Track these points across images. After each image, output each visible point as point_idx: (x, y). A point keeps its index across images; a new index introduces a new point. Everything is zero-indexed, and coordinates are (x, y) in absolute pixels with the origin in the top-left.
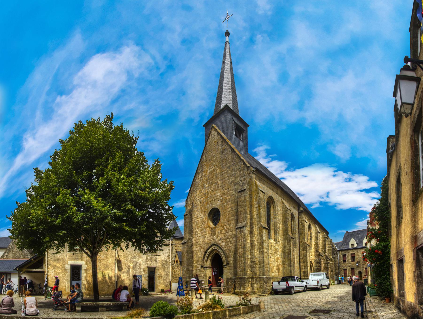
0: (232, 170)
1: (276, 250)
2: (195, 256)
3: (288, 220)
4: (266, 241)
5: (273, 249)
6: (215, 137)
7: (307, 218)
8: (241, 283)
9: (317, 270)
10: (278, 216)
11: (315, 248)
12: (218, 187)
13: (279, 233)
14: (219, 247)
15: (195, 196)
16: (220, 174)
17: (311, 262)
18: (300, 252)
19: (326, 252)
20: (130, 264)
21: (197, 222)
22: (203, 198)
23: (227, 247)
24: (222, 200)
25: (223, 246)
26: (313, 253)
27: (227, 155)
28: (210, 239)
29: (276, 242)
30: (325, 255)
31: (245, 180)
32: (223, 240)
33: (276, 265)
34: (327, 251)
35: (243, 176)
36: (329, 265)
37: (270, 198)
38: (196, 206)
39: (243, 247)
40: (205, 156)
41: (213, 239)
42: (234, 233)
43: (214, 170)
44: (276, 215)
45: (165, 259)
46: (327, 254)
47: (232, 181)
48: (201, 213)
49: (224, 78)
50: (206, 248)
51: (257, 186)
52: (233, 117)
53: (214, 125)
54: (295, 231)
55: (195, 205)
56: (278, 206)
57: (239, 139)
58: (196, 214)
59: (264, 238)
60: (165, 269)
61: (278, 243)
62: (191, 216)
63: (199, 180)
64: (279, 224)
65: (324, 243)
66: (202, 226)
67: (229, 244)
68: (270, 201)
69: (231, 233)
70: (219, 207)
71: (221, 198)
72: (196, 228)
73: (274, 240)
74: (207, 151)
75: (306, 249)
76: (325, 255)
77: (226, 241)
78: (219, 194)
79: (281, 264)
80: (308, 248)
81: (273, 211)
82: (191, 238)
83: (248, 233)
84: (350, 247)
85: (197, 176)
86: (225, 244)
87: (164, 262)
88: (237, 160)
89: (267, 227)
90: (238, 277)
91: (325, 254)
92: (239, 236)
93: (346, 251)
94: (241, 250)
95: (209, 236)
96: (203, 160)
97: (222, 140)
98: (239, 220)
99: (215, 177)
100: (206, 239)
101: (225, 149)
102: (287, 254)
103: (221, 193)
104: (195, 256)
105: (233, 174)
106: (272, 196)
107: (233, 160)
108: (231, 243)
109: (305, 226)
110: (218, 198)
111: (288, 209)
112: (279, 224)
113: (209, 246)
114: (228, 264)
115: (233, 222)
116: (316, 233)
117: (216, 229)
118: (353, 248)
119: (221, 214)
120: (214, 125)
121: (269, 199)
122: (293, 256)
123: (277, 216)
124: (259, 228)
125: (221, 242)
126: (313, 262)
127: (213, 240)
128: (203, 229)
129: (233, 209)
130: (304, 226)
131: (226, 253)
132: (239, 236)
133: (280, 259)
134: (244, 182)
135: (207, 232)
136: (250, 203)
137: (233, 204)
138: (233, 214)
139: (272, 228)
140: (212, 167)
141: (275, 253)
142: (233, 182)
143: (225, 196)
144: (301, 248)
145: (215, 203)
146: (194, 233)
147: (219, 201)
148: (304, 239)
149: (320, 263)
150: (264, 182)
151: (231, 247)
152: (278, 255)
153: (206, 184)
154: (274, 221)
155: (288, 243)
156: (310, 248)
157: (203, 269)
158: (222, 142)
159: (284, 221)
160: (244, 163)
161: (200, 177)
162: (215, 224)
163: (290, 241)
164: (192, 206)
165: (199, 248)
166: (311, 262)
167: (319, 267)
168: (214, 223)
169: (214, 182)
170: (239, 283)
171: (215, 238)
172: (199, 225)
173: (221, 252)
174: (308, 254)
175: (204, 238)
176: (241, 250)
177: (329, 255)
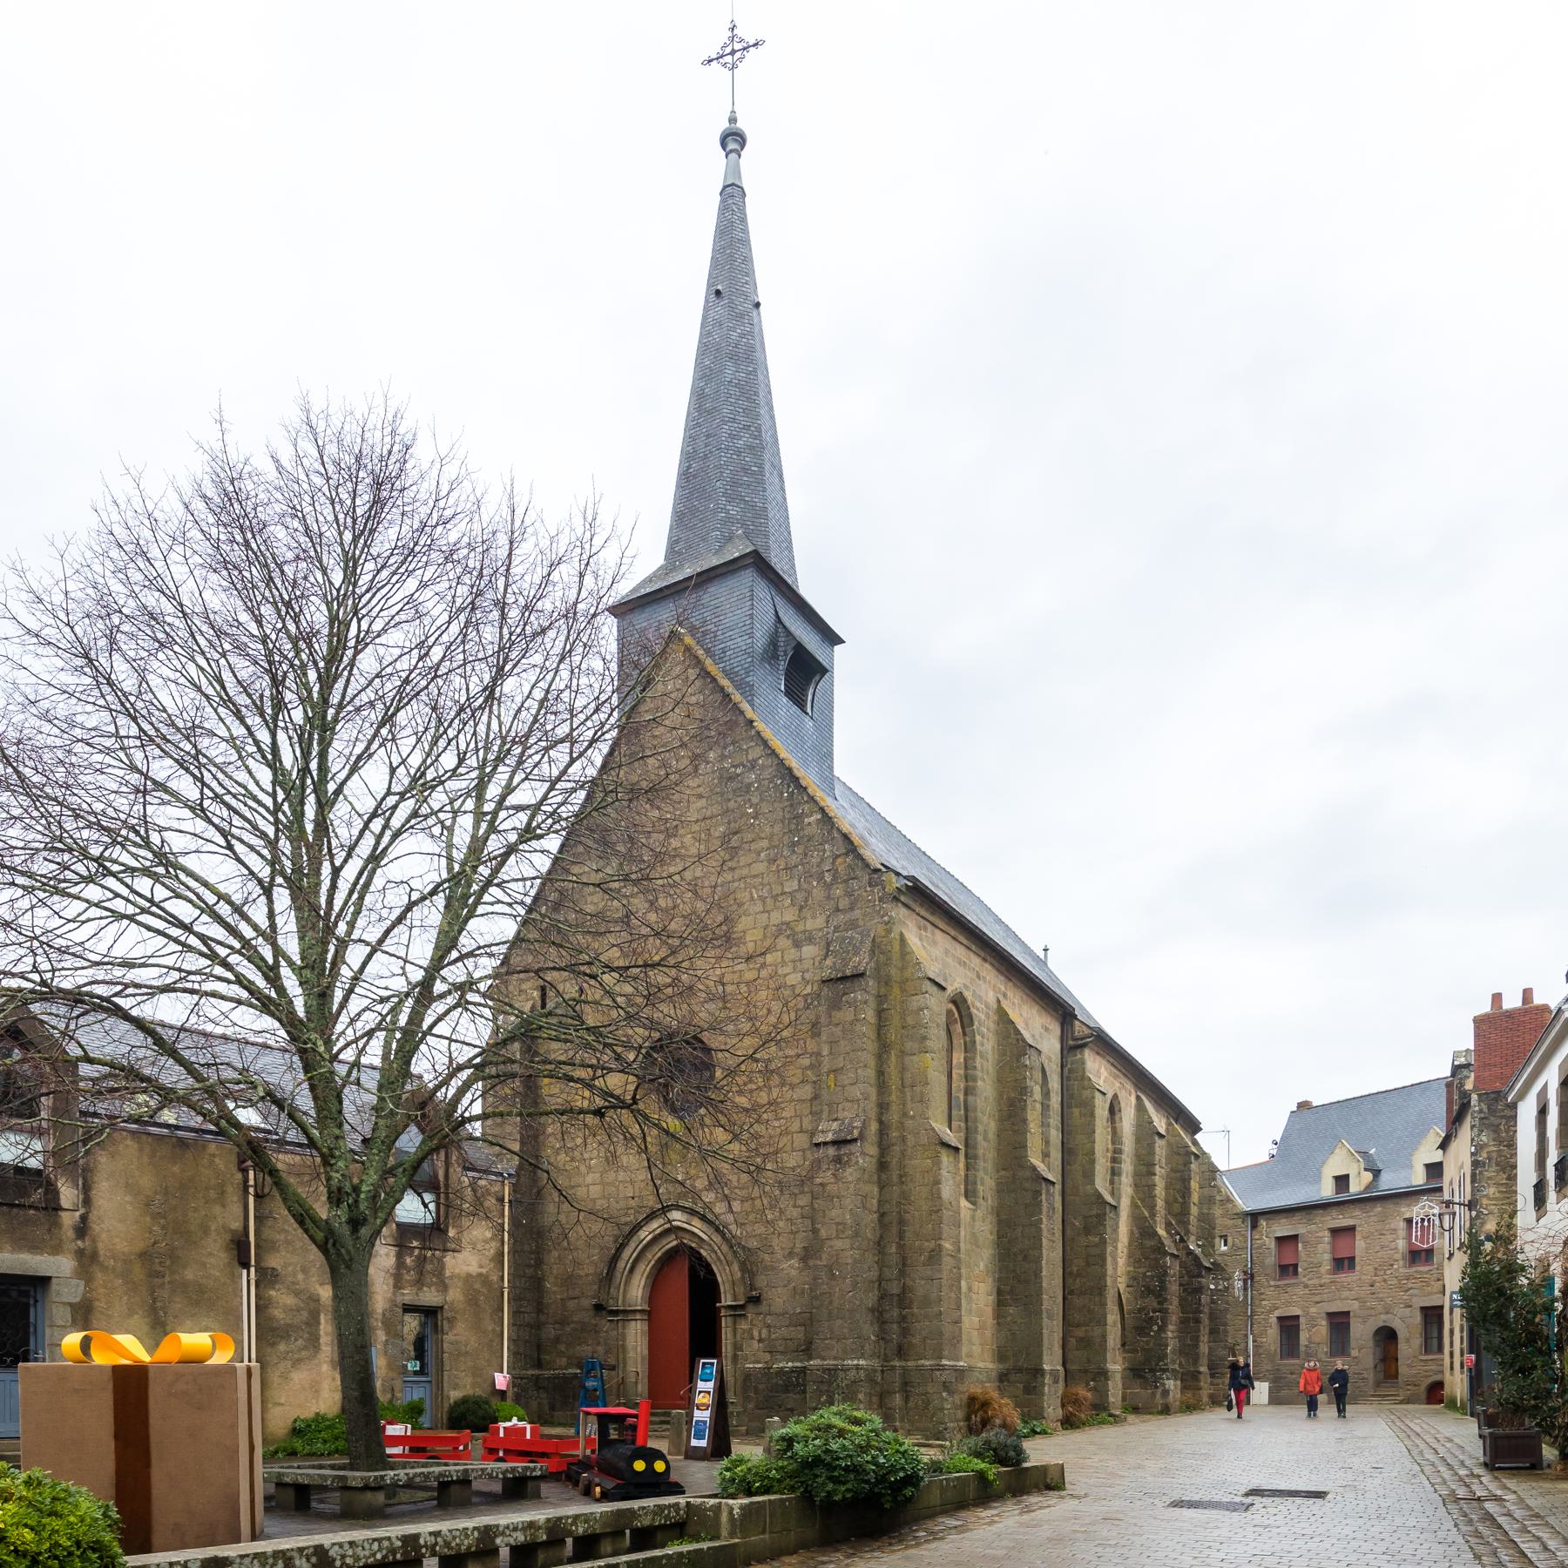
7: (1103, 1070)
19: (1188, 1232)
20: (317, 1286)
36: (598, 1175)
44: (975, 1079)
45: (484, 1271)
52: (778, 599)
57: (799, 711)
60: (884, 1323)
81: (962, 1060)
84: (1327, 1190)
87: (477, 1286)
93: (1298, 1216)
111: (1031, 1046)
118: (1343, 1197)
148: (1089, 1175)
150: (933, 934)
167: (1154, 1312)
174: (1109, 1249)
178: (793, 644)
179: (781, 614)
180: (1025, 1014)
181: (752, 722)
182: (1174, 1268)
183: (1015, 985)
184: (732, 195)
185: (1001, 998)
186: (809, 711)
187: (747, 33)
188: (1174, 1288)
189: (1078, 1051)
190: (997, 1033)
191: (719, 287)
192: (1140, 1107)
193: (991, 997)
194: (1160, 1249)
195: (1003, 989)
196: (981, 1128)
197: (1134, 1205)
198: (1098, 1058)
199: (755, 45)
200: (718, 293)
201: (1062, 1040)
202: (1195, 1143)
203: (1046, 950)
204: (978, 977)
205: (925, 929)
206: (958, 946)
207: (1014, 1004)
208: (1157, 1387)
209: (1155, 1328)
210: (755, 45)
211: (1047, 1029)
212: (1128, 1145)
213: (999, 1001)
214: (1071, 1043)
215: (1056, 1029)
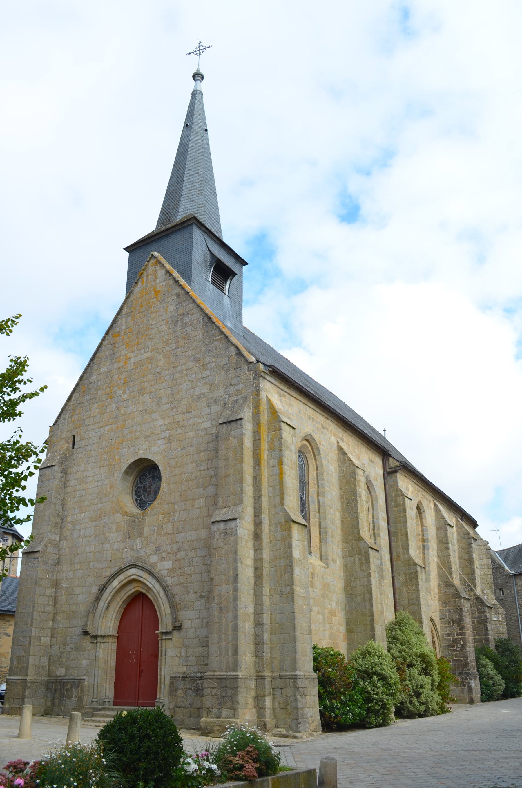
0: (204, 367)
1: (326, 586)
2: (64, 597)
3: (358, 499)
4: (300, 561)
5: (318, 583)
6: (158, 281)
7: (410, 486)
8: (224, 694)
9: (453, 646)
10: (330, 488)
11: (441, 576)
12: (159, 404)
13: (333, 537)
14: (150, 573)
15: (84, 420)
16: (166, 372)
17: (432, 620)
18: (397, 591)
19: (475, 586)
21: (84, 491)
22: (107, 428)
23: (179, 576)
24: (169, 440)
25: (165, 573)
26: (436, 590)
27: (190, 328)
28: (121, 547)
29: (327, 564)
30: (472, 594)
31: (241, 393)
32: (164, 555)
33: (327, 634)
34: (478, 582)
35: (235, 385)
37: (307, 440)
38: (84, 447)
39: (231, 580)
40: (124, 320)
41: (132, 550)
42: (203, 534)
43: (151, 359)
46: (478, 592)
47: (204, 394)
48: (100, 468)
49: (188, 157)
50: (104, 574)
51: (273, 410)
53: (156, 254)
54: (379, 528)
55: (83, 443)
56: (328, 462)
58: (82, 468)
59: (296, 554)
61: (331, 564)
62: (65, 472)
63: (101, 377)
64: (332, 511)
65: (467, 556)
66: (99, 506)
67: (184, 567)
68: (308, 448)
69: (191, 535)
70: (158, 460)
71: (167, 434)
72: (77, 511)
73: (318, 556)
74: (132, 309)
75: (414, 580)
76: (475, 595)
77: (175, 558)
78: (161, 422)
79: (341, 630)
80: (420, 576)
82: (58, 539)
83: (246, 537)
85: (95, 367)
86: (171, 567)
88: (219, 345)
89: (303, 522)
90: (212, 673)
91: (472, 590)
92: (222, 545)
94: (224, 587)
95: (119, 540)
96: (117, 330)
97: (178, 290)
98: (220, 500)
99: (150, 377)
100: (107, 546)
101: (184, 314)
102: (359, 600)
103: (167, 422)
104: (64, 597)
105: (204, 376)
106: (312, 434)
107: (207, 343)
108: (190, 564)
109: (408, 510)
110: (157, 432)
112: (332, 511)
113: (116, 569)
114: (178, 628)
115: (200, 503)
116: (441, 528)
117: (144, 520)
119: (163, 479)
120: (156, 254)
121: (305, 442)
122: (379, 606)
123: (327, 489)
124: (281, 523)
125: (157, 559)
126: (437, 620)
127: (132, 553)
128: (100, 516)
129: (202, 468)
130: (404, 510)
131: (174, 596)
132: (222, 545)
133: (337, 614)
134: (237, 400)
135: (114, 527)
136: (253, 454)
137: (203, 454)
138: (201, 480)
139: (314, 521)
140: (145, 352)
141: (324, 596)
142: (206, 397)
143: (179, 431)
144: (400, 579)
145: (146, 446)
146: (70, 526)
147: (160, 442)
148: (406, 548)
149: (460, 622)
151: (190, 575)
152: (334, 604)
153: (121, 392)
154: (318, 501)
155: (361, 564)
156: (427, 574)
157: (87, 642)
158: (178, 295)
159: (348, 503)
160: (239, 353)
161: (104, 369)
162: (142, 504)
163: (367, 558)
164: (71, 445)
165: (80, 573)
166: (432, 620)
167: (458, 635)
168: (137, 500)
169: (147, 390)
170: (216, 695)
171: (138, 543)
172: (87, 503)
173: (156, 588)
175: (102, 544)
176: (224, 587)
177: (485, 594)
178: (216, 259)
179: (209, 247)
180: (357, 452)
181: (188, 293)
182: (466, 606)
183: (349, 435)
184: (195, 95)
185: (339, 440)
186: (227, 293)
187: (205, 44)
188: (468, 620)
189: (393, 475)
190: (339, 461)
191: (188, 124)
192: (437, 510)
193: (333, 440)
194: (457, 595)
195: (341, 436)
196: (329, 517)
197: (439, 568)
198: (406, 480)
199: (209, 47)
200: (187, 125)
201: (384, 470)
202: (476, 533)
203: (384, 431)
204: (323, 427)
205: (285, 396)
206: (308, 408)
207: (349, 445)
208: (465, 685)
209: (459, 646)
210: (209, 47)
211: (373, 462)
212: (432, 533)
213: (338, 442)
214: (388, 470)
215: (379, 461)
